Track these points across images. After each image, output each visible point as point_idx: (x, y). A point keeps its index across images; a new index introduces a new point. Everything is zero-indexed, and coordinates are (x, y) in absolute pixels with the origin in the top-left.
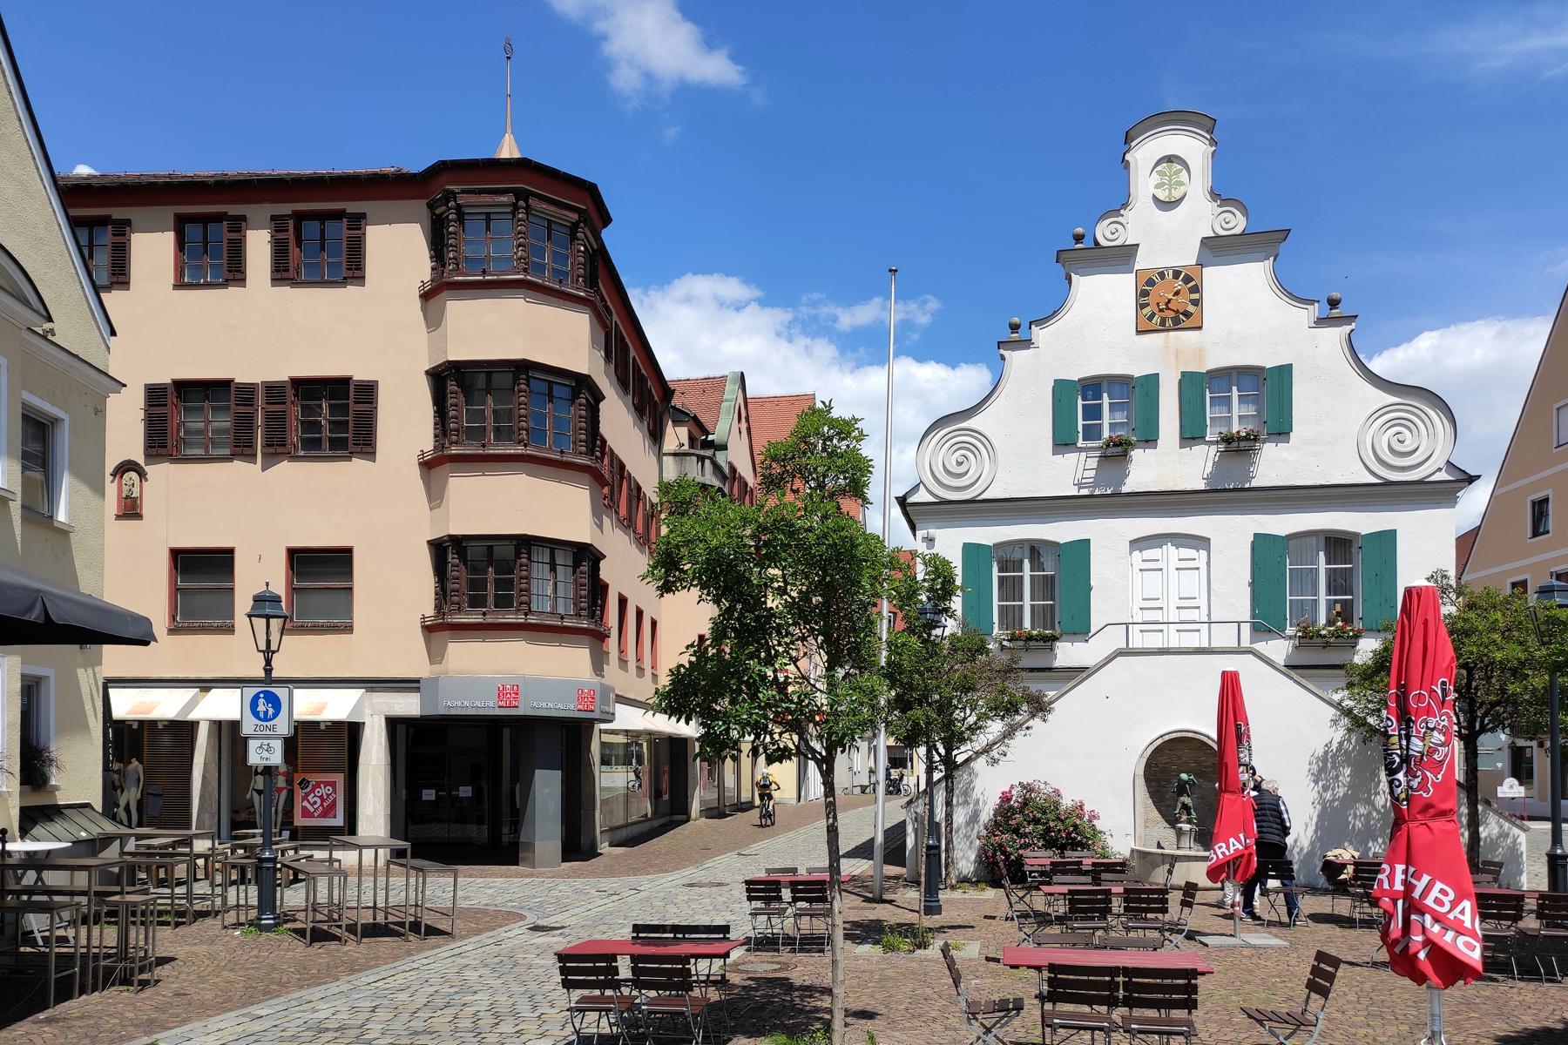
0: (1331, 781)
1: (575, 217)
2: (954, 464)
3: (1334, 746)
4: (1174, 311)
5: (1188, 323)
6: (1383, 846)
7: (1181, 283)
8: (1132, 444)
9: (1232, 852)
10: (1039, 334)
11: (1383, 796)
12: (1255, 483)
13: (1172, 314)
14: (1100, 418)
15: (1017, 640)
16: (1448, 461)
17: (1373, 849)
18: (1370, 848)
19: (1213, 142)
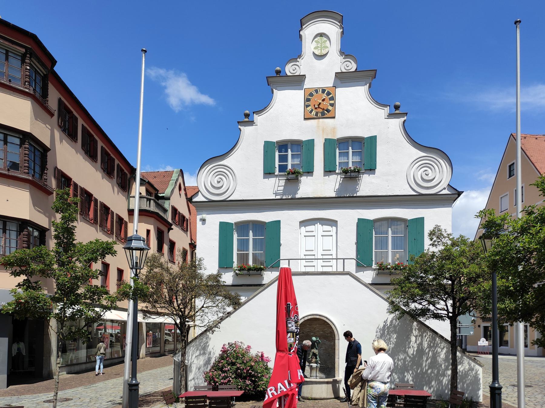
0: (387, 341)
1: (24, 50)
2: (216, 182)
3: (388, 323)
4: (322, 109)
5: (328, 115)
6: (412, 375)
7: (325, 95)
8: (300, 173)
9: (279, 392)
10: (257, 118)
11: (412, 349)
12: (359, 194)
13: (321, 110)
14: (287, 161)
15: (243, 270)
16: (449, 185)
17: (407, 376)
18: (406, 376)
19: (341, 27)
